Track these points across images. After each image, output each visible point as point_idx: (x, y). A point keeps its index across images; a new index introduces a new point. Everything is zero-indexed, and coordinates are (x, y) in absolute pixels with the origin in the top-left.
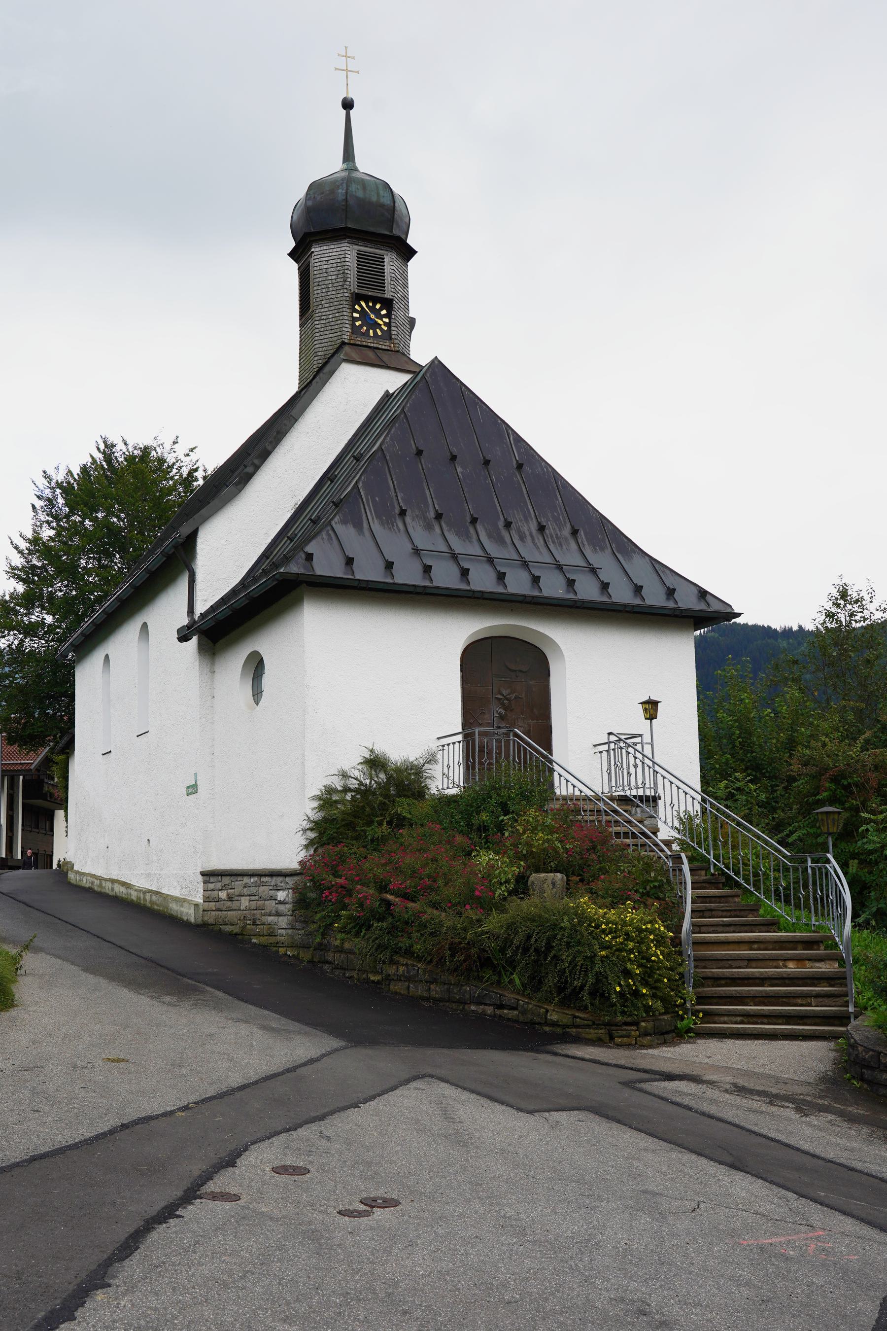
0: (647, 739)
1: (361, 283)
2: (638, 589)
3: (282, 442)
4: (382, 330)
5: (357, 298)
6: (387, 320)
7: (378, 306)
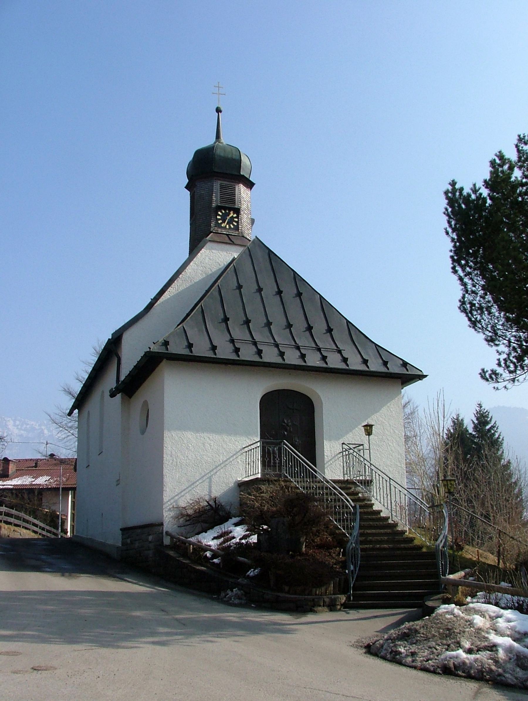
0: (366, 446)
2: (365, 362)
3: (156, 370)
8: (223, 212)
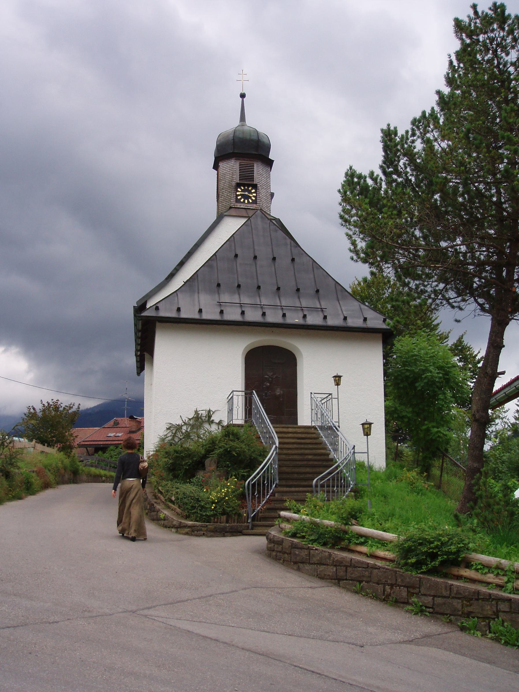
0: (335, 395)
1: (241, 177)
4: (252, 200)
5: (238, 185)
6: (255, 195)
7: (250, 189)
8: (243, 188)
